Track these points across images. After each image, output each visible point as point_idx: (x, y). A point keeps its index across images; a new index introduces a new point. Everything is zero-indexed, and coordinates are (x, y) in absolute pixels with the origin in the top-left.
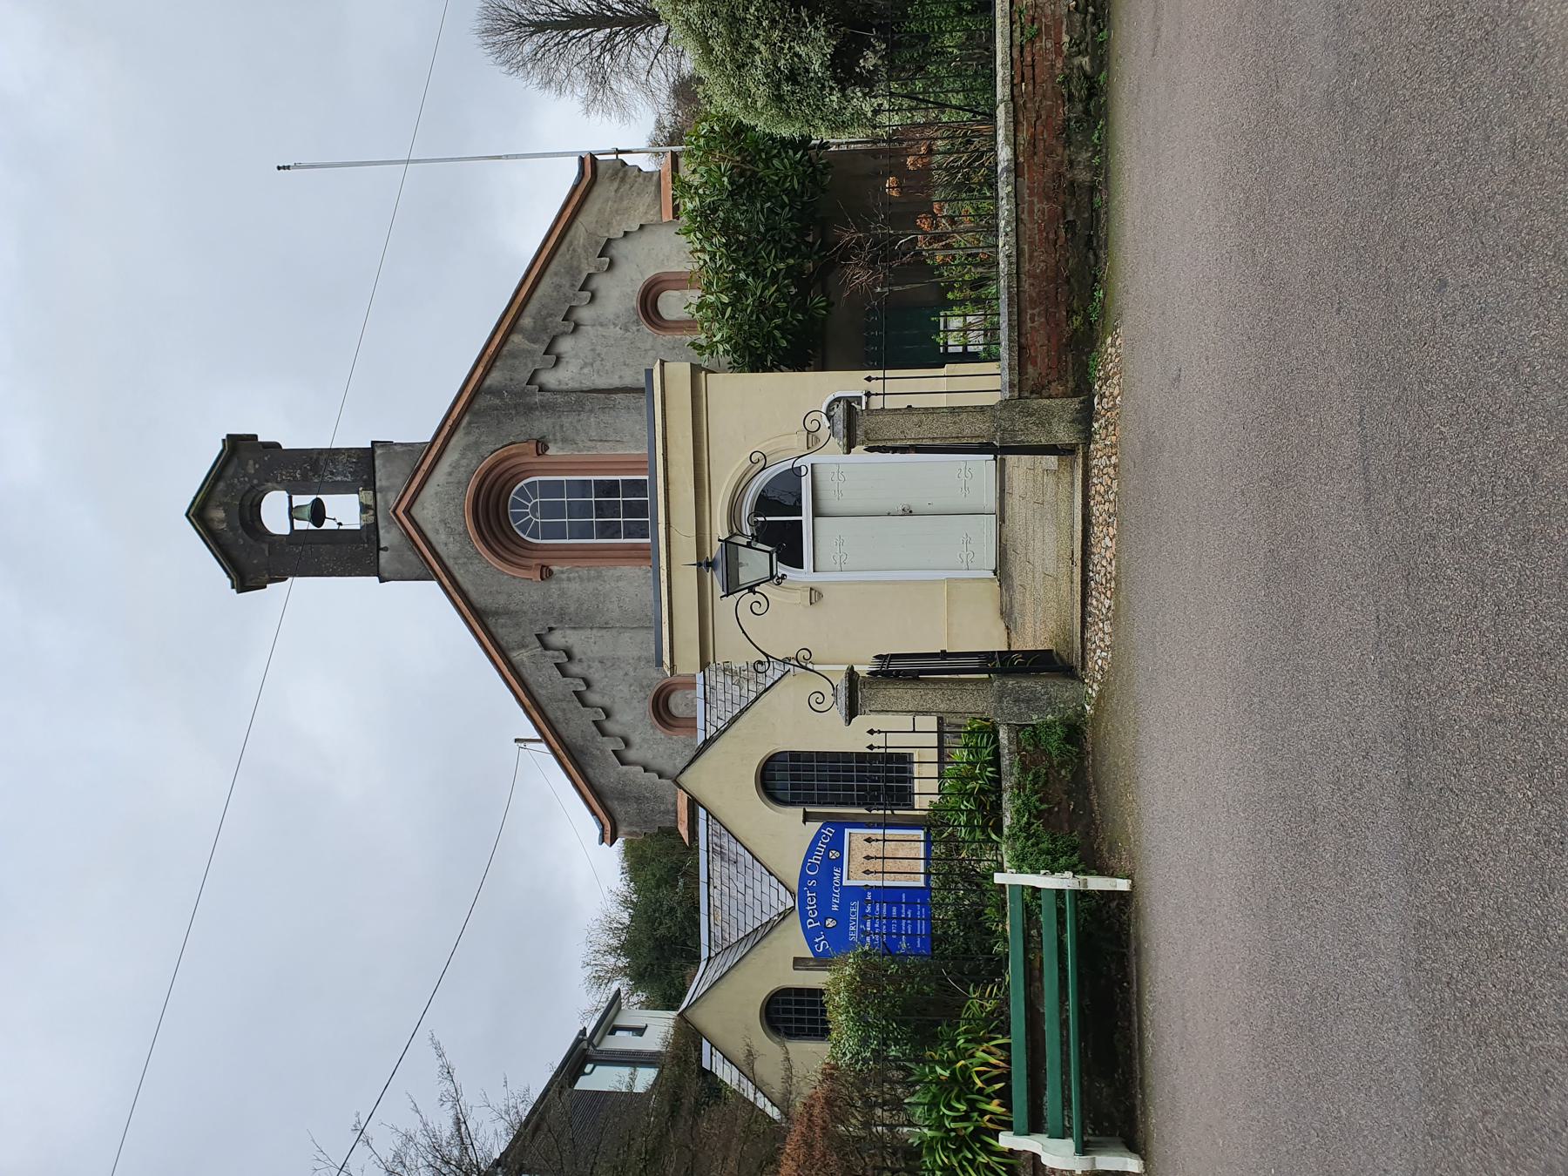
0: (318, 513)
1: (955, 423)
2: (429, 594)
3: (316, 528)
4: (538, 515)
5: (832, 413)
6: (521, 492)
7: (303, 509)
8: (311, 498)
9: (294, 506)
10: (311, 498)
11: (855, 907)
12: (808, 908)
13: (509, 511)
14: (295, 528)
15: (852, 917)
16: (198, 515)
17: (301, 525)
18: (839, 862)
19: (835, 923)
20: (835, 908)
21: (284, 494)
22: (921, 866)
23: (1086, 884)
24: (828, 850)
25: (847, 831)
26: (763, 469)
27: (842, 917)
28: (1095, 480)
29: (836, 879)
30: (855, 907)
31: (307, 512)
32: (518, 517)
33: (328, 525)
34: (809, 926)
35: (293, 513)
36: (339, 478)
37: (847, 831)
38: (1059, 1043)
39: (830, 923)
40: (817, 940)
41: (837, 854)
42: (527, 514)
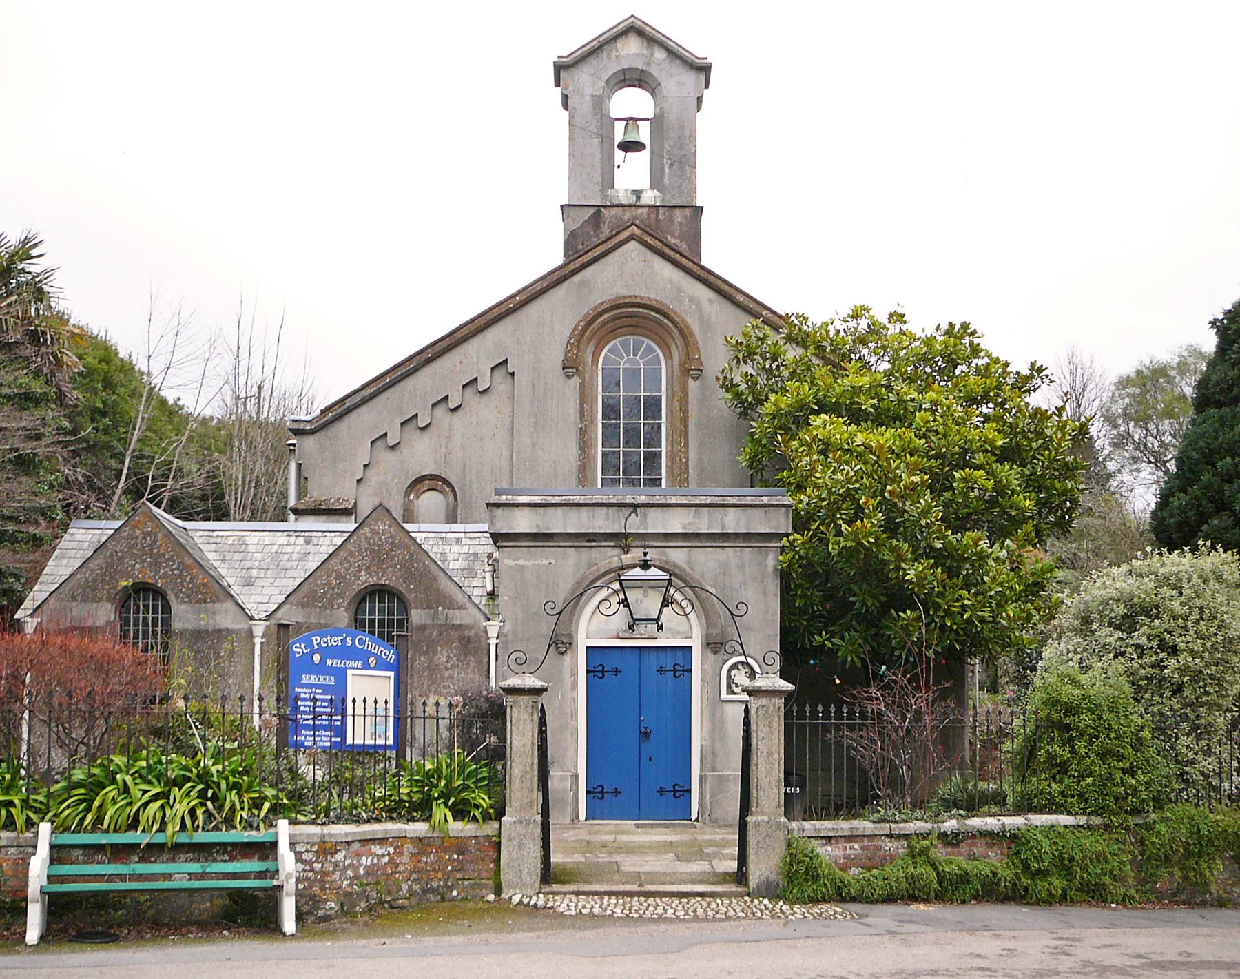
0: (630, 146)
1: (770, 783)
2: (554, 257)
3: (616, 144)
4: (627, 366)
5: (740, 667)
6: (649, 350)
7: (635, 132)
8: (647, 142)
9: (638, 122)
10: (647, 142)
11: (330, 680)
12: (329, 638)
13: (632, 337)
14: (616, 122)
15: (322, 679)
16: (632, 27)
17: (619, 127)
18: (366, 666)
19: (317, 662)
20: (329, 662)
21: (651, 116)
22: (359, 741)
23: (288, 895)
24: (375, 656)
25: (392, 674)
26: (732, 614)
27: (321, 669)
28: (621, 901)
29: (352, 664)
30: (330, 680)
31: (632, 137)
32: (626, 346)
33: (619, 154)
34: (314, 638)
35: (631, 121)
36: (667, 170)
37: (392, 674)
38: (867, 906)
39: (317, 658)
40: (303, 646)
41: (372, 665)
42: (628, 354)
